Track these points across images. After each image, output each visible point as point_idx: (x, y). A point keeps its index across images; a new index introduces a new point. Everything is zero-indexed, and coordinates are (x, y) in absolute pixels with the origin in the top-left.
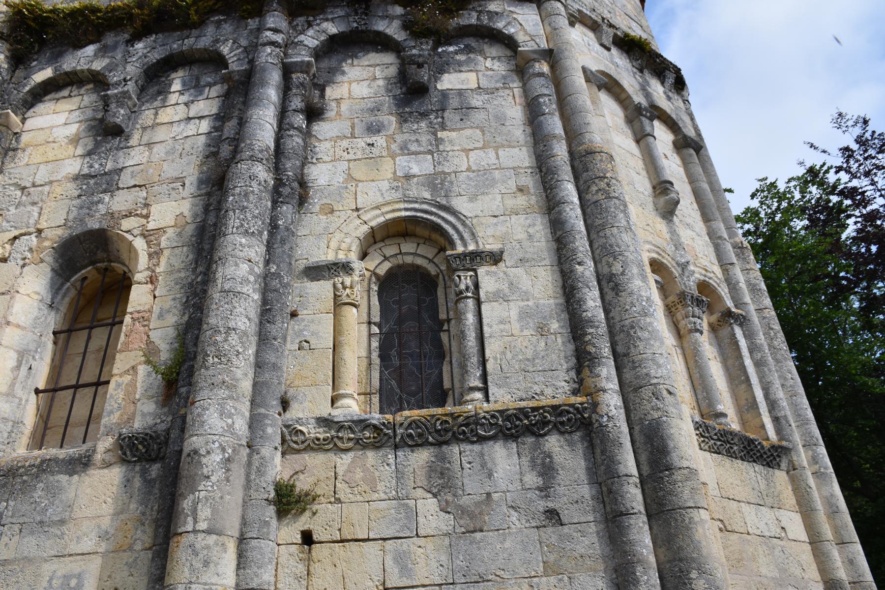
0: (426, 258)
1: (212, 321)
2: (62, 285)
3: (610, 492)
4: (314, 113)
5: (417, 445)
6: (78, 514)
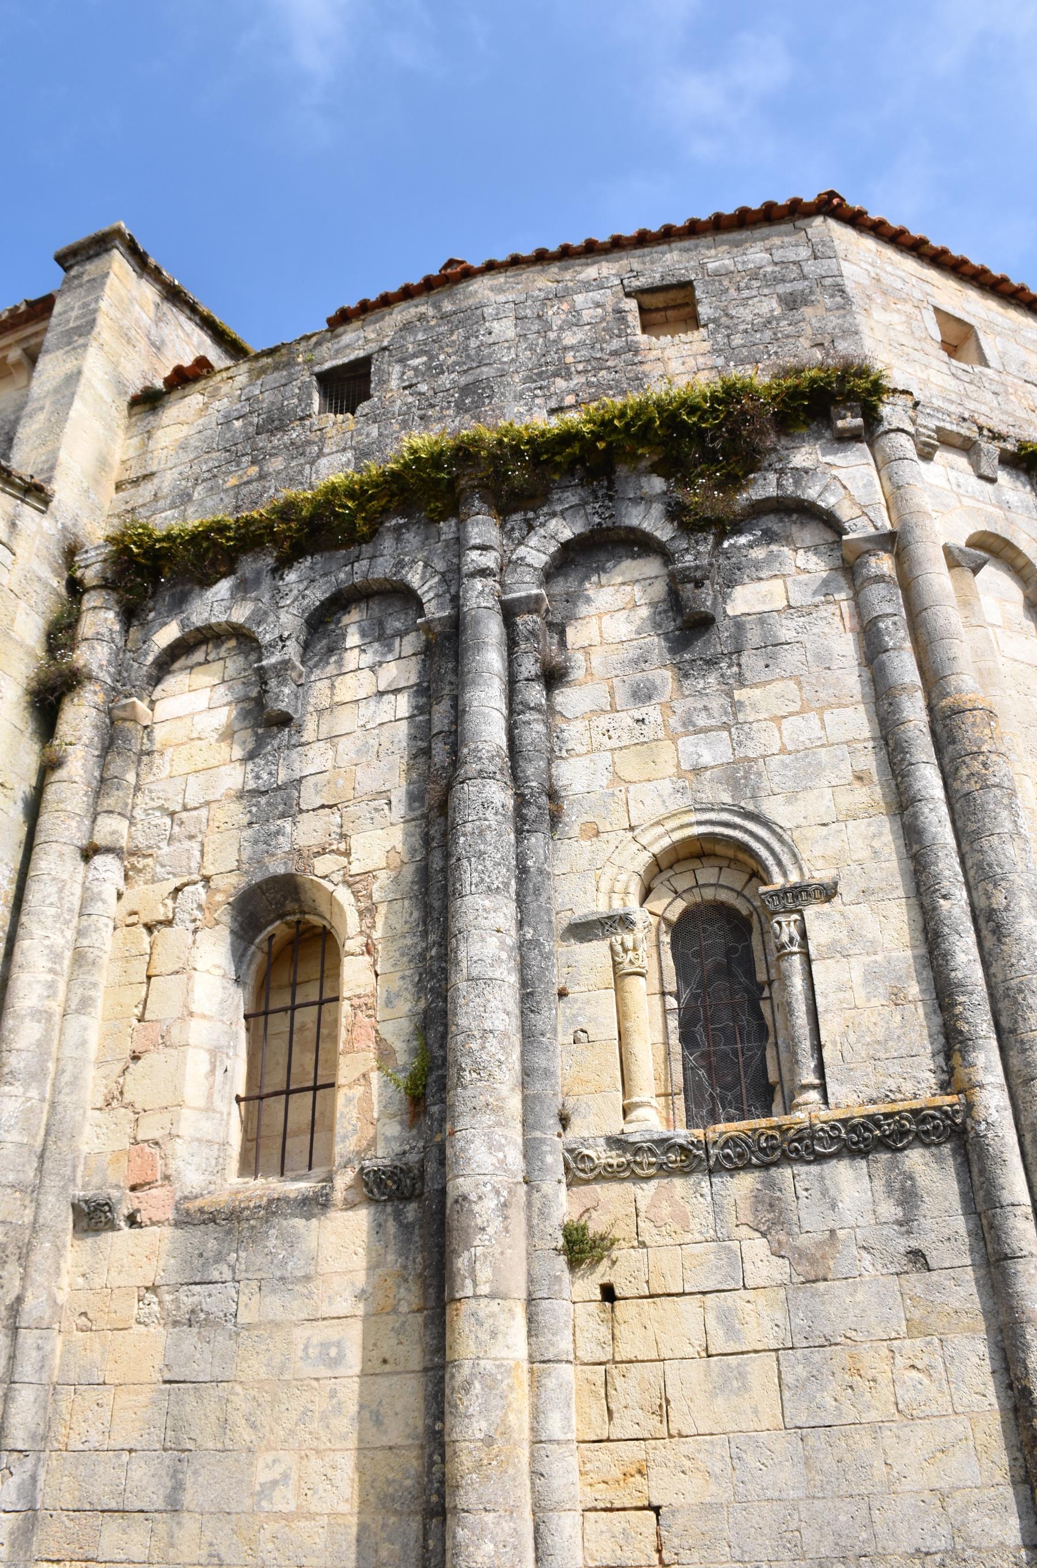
0: (732, 890)
1: (463, 1021)
2: (246, 949)
3: (992, 1227)
4: (553, 677)
5: (738, 1169)
6: (324, 1268)
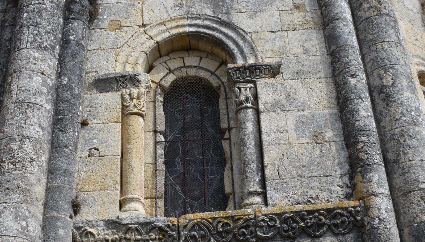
0: (208, 71)
